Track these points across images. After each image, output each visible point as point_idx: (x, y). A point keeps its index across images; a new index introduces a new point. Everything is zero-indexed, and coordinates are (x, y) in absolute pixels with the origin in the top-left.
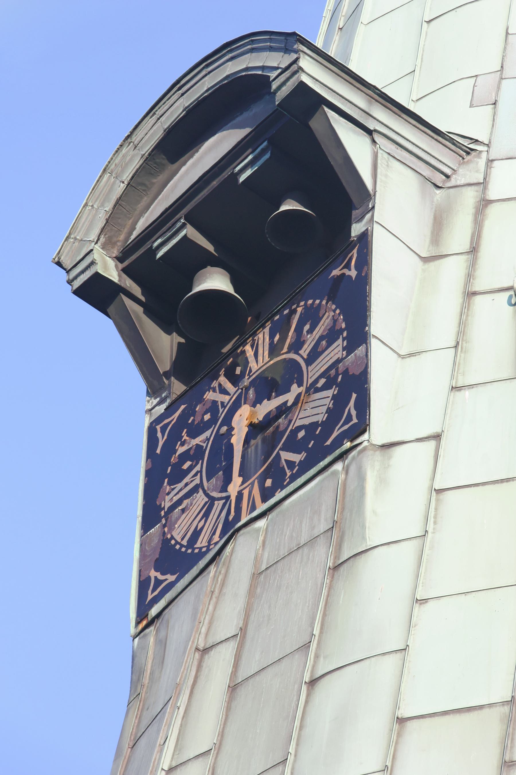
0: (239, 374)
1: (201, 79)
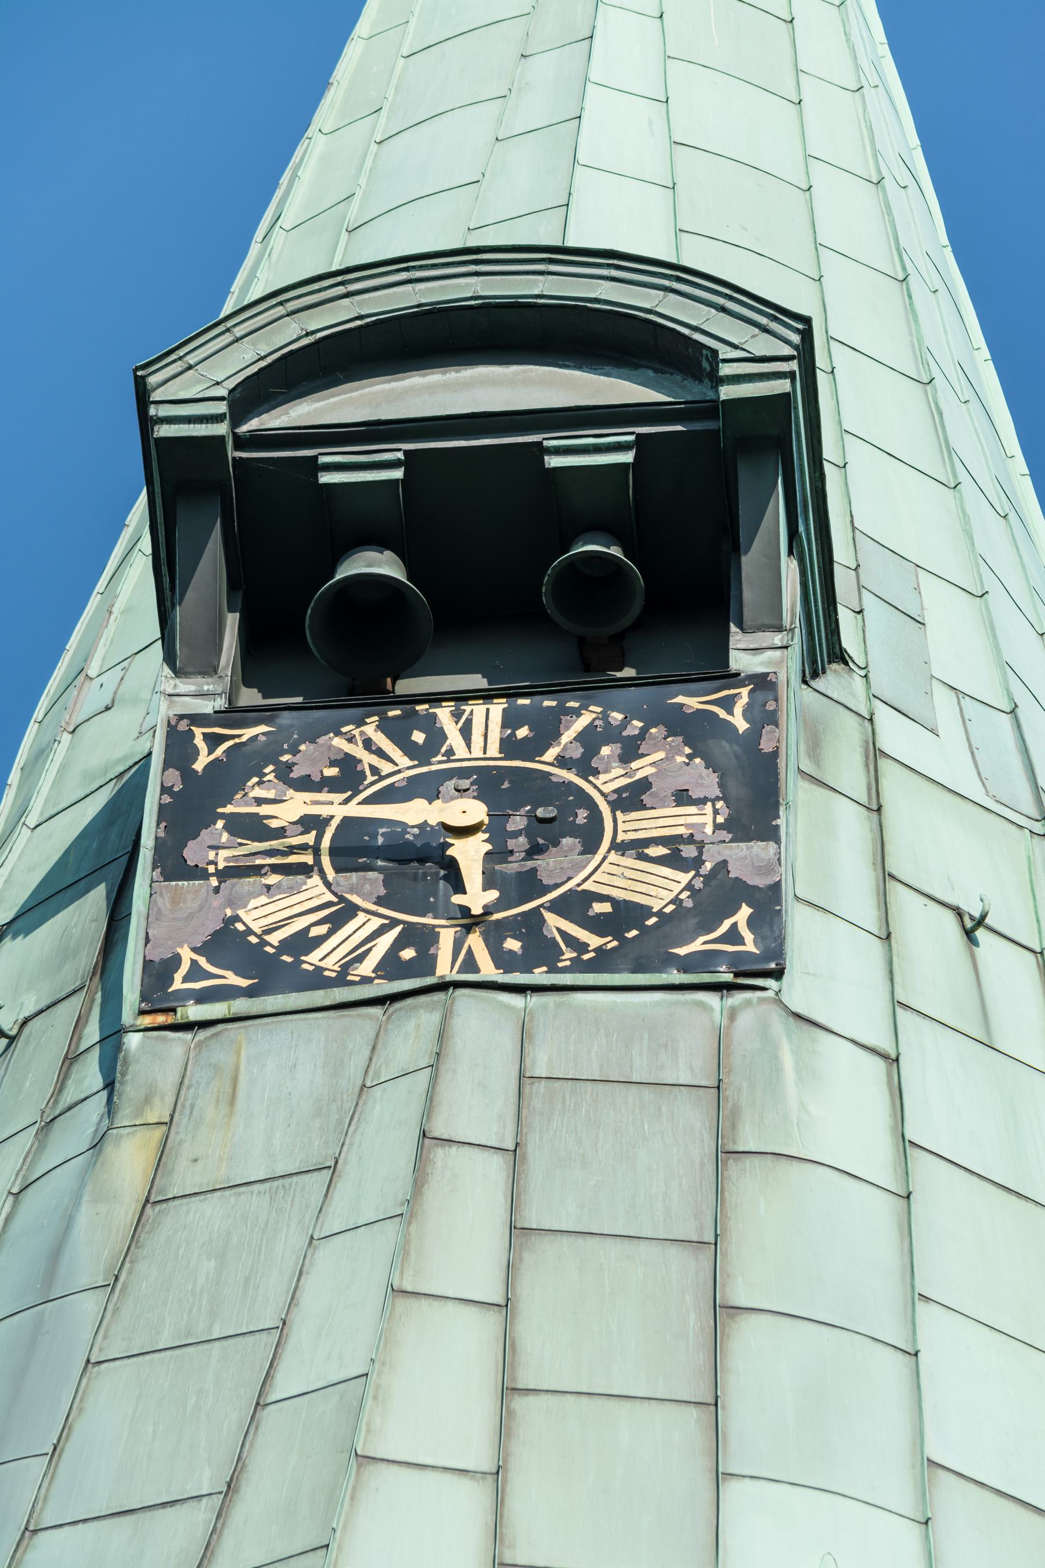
0: (413, 738)
1: (527, 273)
